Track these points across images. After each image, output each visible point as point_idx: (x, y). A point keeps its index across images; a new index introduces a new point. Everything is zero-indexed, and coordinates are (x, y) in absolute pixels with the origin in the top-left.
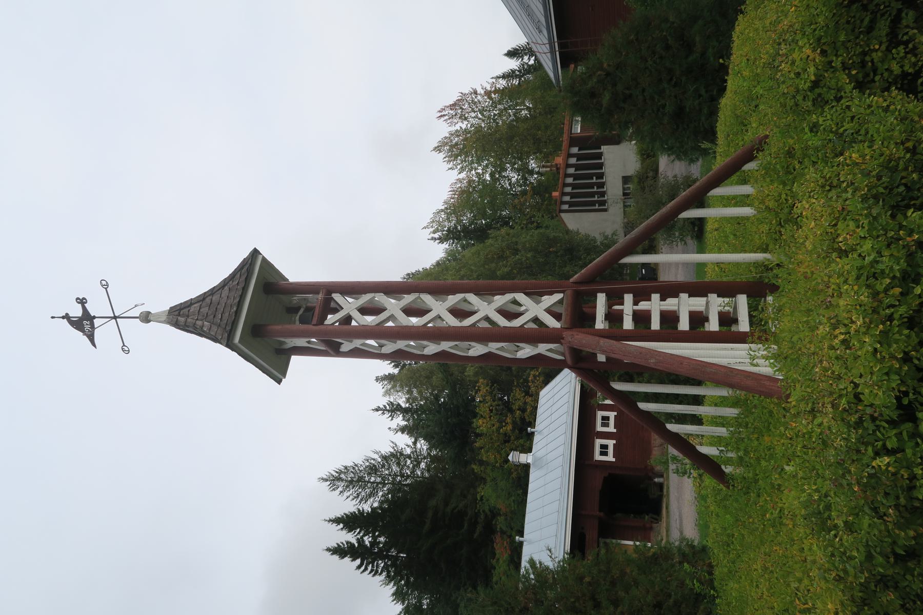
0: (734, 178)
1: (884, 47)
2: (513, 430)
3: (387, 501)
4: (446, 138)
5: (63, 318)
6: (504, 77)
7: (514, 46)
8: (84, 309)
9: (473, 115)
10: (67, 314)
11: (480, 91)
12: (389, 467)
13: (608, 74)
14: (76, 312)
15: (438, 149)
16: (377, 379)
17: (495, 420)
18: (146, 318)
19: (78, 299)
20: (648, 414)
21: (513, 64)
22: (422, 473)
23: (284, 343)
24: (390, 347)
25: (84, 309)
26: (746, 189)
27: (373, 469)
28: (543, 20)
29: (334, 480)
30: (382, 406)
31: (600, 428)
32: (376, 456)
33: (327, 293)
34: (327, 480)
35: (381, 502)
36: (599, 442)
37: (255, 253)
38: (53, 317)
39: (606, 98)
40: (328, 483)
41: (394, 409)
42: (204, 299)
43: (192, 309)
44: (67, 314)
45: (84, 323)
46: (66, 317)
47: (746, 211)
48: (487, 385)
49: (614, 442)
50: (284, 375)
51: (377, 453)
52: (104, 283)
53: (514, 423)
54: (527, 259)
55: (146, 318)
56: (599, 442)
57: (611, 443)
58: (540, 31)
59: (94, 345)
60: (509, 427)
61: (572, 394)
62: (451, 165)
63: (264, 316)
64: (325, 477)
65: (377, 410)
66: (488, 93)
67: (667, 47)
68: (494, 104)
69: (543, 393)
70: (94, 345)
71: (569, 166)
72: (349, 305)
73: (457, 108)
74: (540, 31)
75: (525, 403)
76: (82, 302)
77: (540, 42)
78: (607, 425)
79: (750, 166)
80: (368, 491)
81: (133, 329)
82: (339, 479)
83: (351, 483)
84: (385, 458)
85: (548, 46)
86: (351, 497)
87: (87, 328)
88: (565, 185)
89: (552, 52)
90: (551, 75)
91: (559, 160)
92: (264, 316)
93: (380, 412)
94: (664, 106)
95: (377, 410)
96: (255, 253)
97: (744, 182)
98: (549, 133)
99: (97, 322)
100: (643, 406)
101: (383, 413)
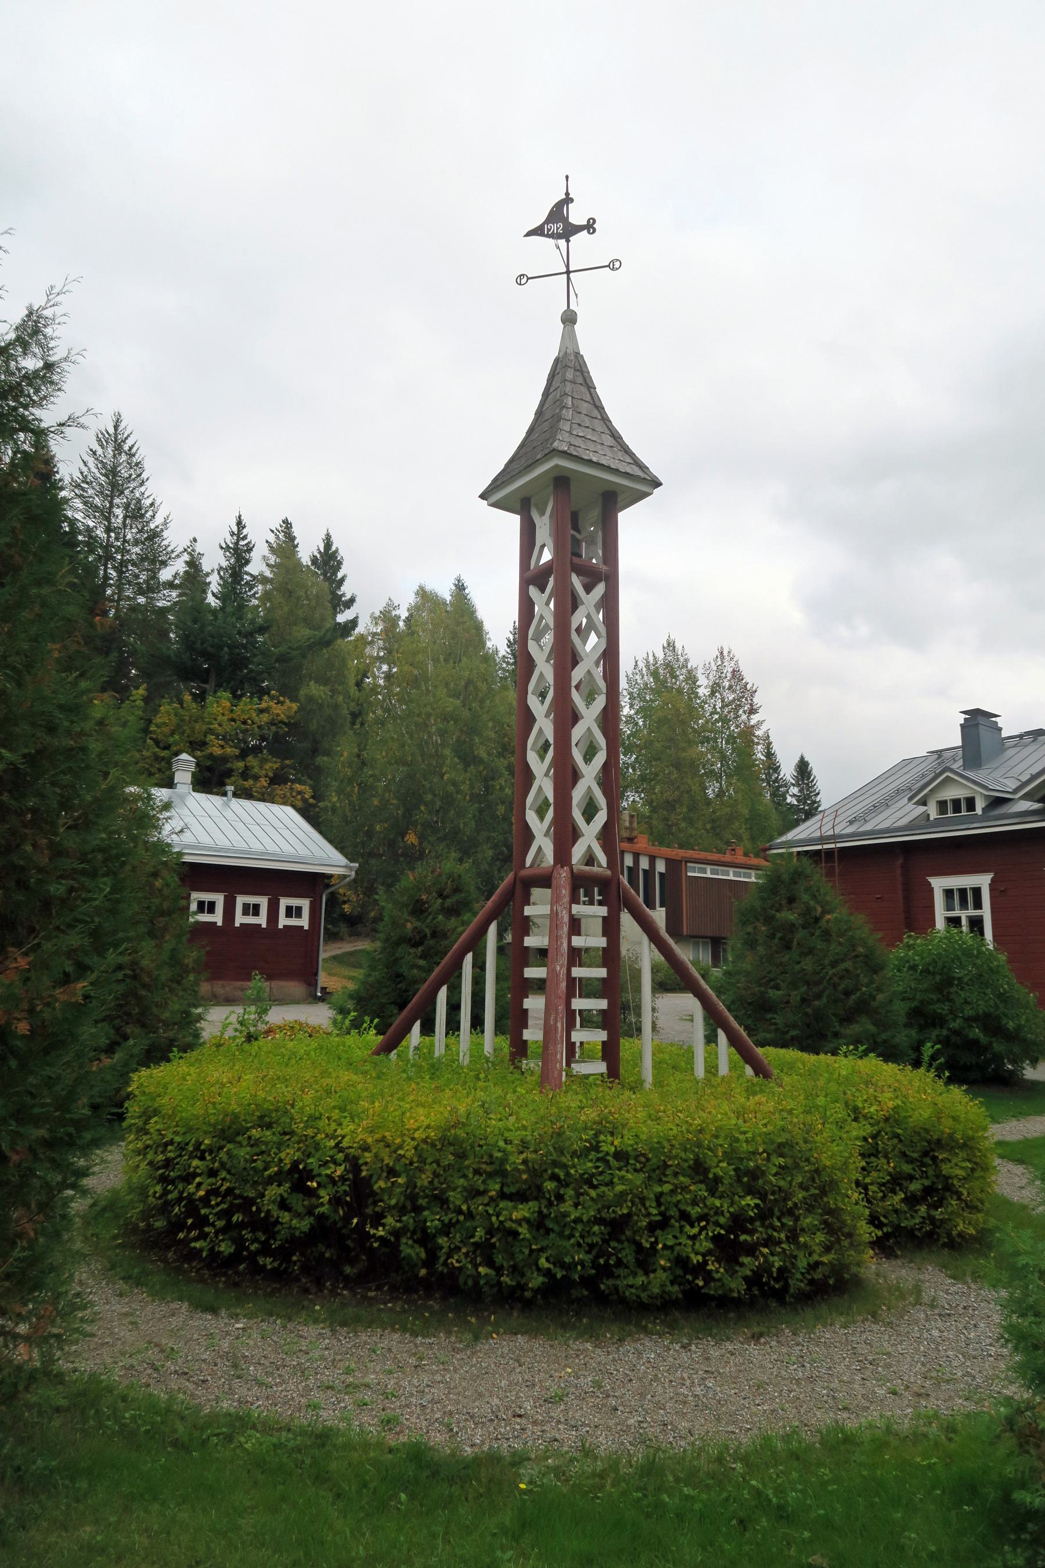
0: (737, 1057)
1: (891, 1170)
2: (211, 756)
3: (74, 531)
4: (687, 661)
5: (567, 194)
6: (769, 754)
7: (814, 772)
8: (578, 229)
9: (719, 705)
10: (572, 200)
11: (754, 719)
12: (136, 542)
13: (817, 920)
14: (576, 216)
15: (670, 646)
16: (287, 524)
17: (228, 727)
18: (569, 319)
19: (594, 221)
20: (458, 965)
21: (788, 771)
22: (129, 598)
23: (542, 513)
24: (541, 650)
25: (578, 229)
26: (724, 1069)
27: (136, 513)
28: (868, 827)
29: (116, 441)
30: (245, 532)
31: (241, 900)
32: (159, 520)
33: (605, 576)
34: (116, 427)
35: (72, 522)
36: (263, 901)
37: (657, 484)
38: (567, 177)
39: (790, 916)
40: (112, 431)
41: (239, 552)
42: (597, 407)
43: (584, 389)
44: (572, 200)
45: (558, 224)
46: (568, 200)
47: (700, 1072)
48: (288, 717)
49: (220, 924)
50: (494, 505)
51: (165, 523)
52: (617, 264)
53: (224, 759)
54: (502, 789)
55: (569, 319)
56: (263, 901)
57: (262, 920)
58: (851, 822)
59: (529, 234)
60: (218, 751)
61: (210, 849)
62: (641, 665)
63: (571, 487)
64: (122, 426)
65: (240, 523)
66: (748, 732)
67: (847, 993)
68: (731, 740)
69: (289, 810)
70: (529, 234)
71: (636, 856)
72: (590, 600)
73: (738, 691)
74: (851, 822)
75: (256, 778)
76: (590, 227)
77: (838, 820)
78: (245, 913)
79: (749, 1071)
80: (97, 501)
81: (552, 297)
82: (118, 448)
83: (112, 472)
84: (155, 535)
85: (831, 833)
86: (85, 470)
87: (554, 228)
88: (652, 860)
89: (822, 839)
90: (790, 836)
91: (642, 842)
92: (571, 487)
93: (235, 529)
94: (777, 987)
95: (240, 523)
96: (657, 484)
97: (733, 1067)
98: (683, 825)
99: (562, 243)
100: (469, 957)
101: (232, 534)
